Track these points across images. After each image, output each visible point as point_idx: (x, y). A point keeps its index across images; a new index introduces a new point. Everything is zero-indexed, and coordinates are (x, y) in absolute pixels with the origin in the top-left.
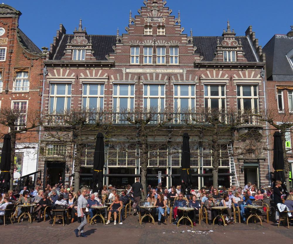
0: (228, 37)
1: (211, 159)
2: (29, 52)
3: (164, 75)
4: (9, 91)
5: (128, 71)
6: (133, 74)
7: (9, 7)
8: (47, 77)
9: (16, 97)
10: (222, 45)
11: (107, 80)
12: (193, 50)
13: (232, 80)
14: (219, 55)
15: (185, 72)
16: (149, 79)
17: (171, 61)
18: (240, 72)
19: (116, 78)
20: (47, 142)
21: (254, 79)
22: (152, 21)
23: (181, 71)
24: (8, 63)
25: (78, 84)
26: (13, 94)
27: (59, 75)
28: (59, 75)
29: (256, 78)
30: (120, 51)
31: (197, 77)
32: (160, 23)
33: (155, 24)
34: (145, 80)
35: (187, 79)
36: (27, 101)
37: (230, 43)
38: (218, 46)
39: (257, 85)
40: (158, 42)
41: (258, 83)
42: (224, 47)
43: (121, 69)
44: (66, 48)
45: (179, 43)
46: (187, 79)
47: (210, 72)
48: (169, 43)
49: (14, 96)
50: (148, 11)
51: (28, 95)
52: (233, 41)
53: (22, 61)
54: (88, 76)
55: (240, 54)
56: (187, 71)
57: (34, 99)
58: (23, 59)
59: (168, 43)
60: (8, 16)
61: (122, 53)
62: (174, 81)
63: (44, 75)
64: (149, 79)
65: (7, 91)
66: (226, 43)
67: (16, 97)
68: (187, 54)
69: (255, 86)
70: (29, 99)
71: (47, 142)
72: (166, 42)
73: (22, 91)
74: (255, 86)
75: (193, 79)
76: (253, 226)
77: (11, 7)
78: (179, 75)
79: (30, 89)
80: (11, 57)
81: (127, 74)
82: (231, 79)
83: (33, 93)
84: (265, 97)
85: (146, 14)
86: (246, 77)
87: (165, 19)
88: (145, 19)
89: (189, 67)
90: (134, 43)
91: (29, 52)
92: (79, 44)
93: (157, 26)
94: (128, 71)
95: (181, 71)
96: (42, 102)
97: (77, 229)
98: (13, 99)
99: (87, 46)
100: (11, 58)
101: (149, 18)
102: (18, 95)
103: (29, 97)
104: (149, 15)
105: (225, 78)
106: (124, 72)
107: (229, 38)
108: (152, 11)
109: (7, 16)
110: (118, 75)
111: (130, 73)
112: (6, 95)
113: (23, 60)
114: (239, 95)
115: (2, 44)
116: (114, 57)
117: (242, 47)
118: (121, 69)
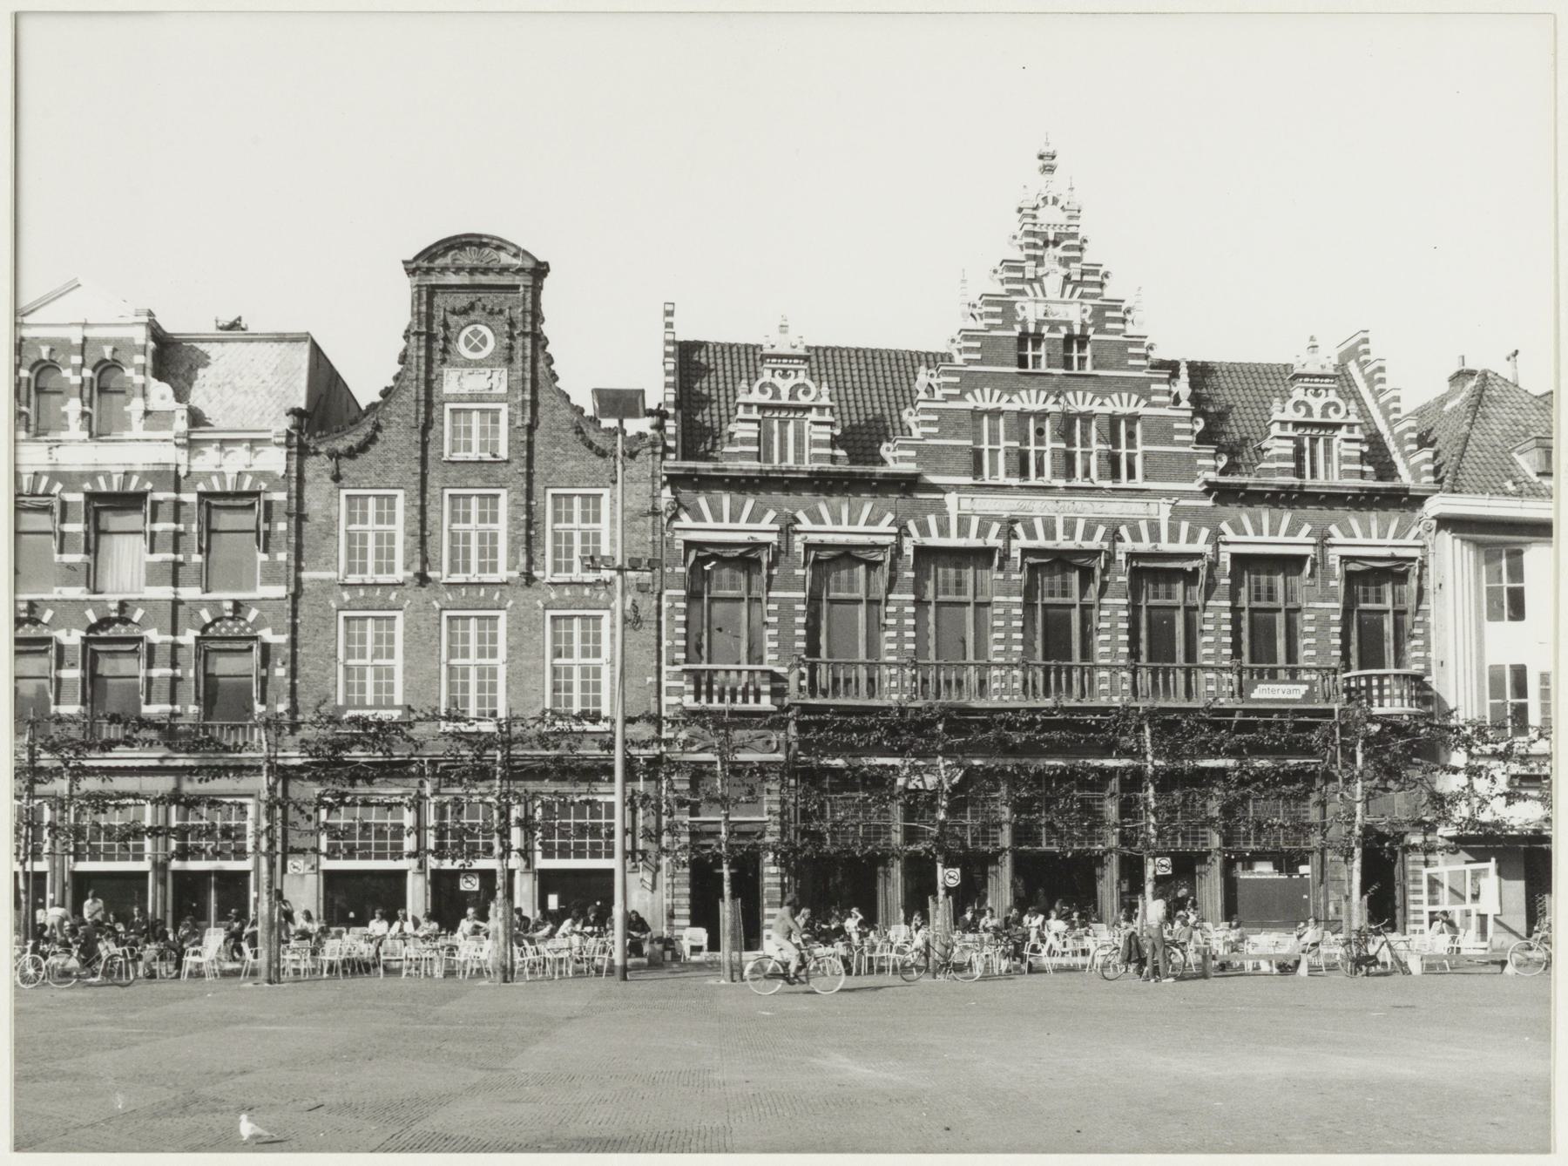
1: (1149, 758)
8: (676, 524)
12: (1192, 432)
17: (1169, 480)
27: (1367, 534)
28: (1367, 534)
29: (1295, 535)
35: (1174, 536)
40: (1066, 399)
44: (1366, 449)
46: (1174, 536)
47: (1272, 518)
52: (1327, 400)
54: (1353, 536)
59: (1056, 402)
75: (1192, 538)
76: (156, 986)
82: (1323, 542)
86: (840, 523)
97: (1307, 863)
99: (814, 410)
102: (362, 592)
103: (401, 597)
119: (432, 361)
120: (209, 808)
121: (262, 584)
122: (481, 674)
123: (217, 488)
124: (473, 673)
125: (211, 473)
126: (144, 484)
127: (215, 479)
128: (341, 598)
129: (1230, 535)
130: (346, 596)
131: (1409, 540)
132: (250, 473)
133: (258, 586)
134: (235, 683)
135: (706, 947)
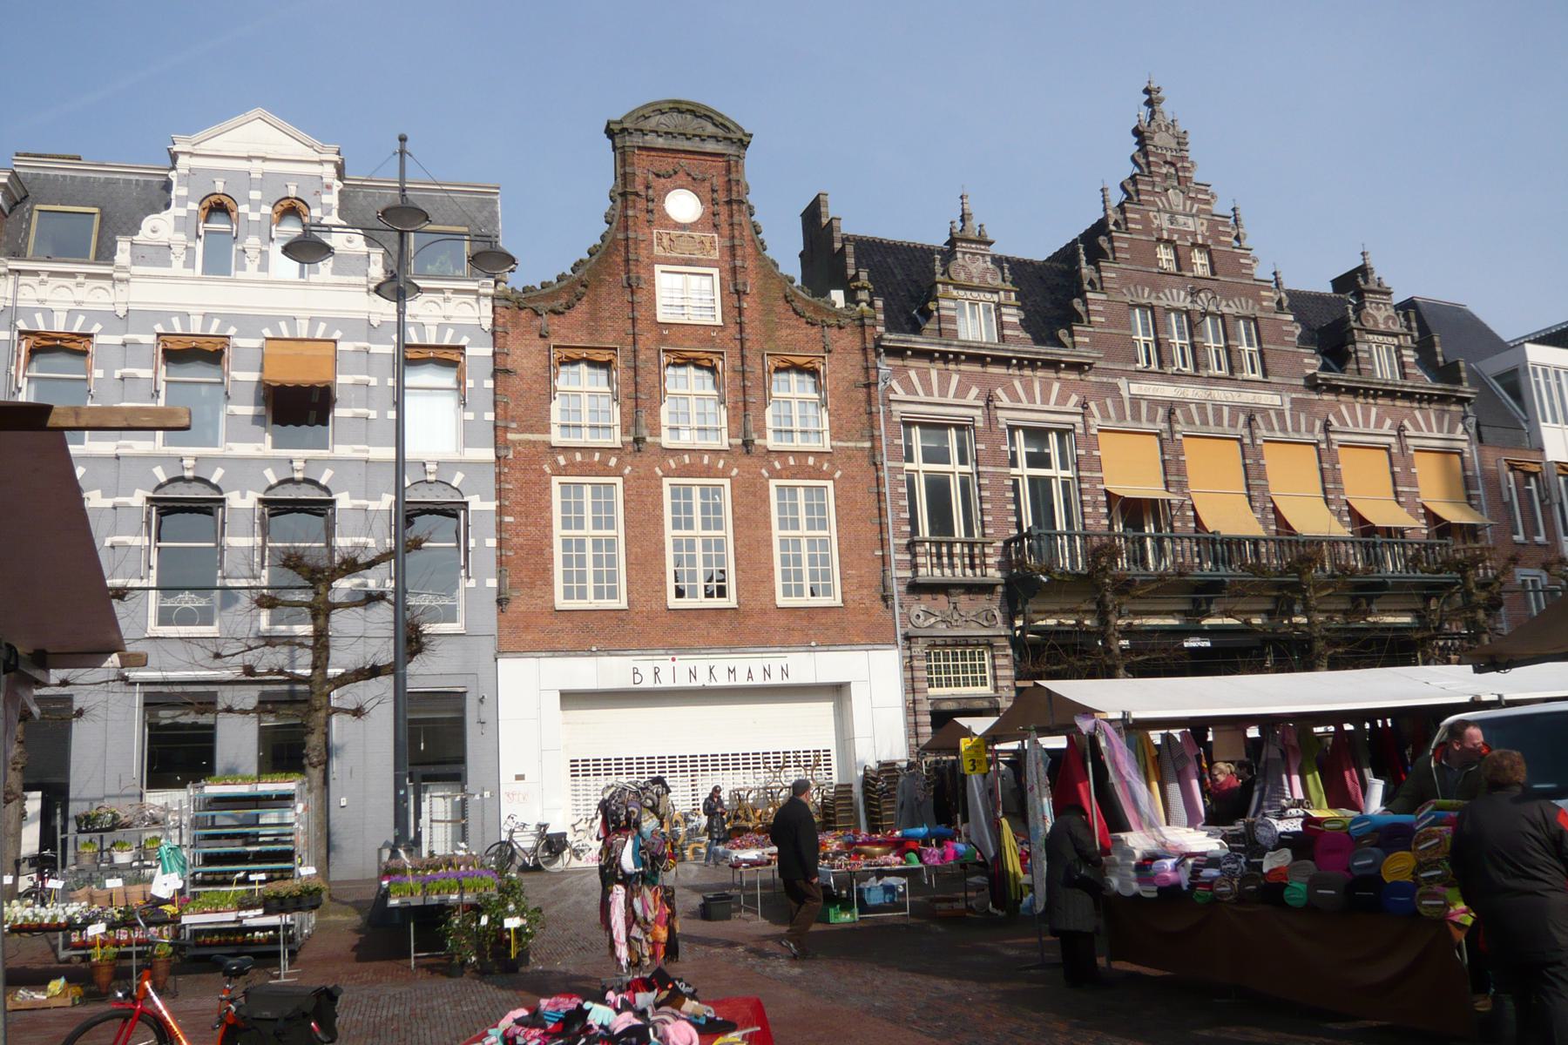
0: (971, 253)
2: (807, 297)
3: (1235, 409)
4: (756, 442)
5: (1135, 389)
6: (1154, 403)
7: (712, 115)
9: (786, 467)
10: (952, 279)
11: (1079, 418)
13: (1403, 438)
14: (943, 312)
15: (1287, 406)
16: (1197, 422)
18: (1417, 413)
19: (1105, 415)
20: (929, 641)
21: (1057, 408)
22: (1172, 223)
23: (1276, 400)
24: (733, 330)
25: (993, 429)
26: (774, 455)
30: (1103, 320)
31: (1318, 424)
32: (1194, 234)
33: (1183, 235)
34: (1187, 423)
36: (727, 482)
37: (1381, 320)
38: (940, 283)
39: (1068, 431)
41: (1074, 425)
42: (958, 287)
43: (1115, 381)
45: (1257, 307)
48: (1231, 303)
49: (777, 465)
50: (1157, 190)
51: (829, 461)
53: (789, 331)
54: (1020, 401)
55: (1012, 316)
56: (1293, 401)
57: (853, 478)
58: (790, 322)
60: (710, 146)
61: (1109, 327)
62: (1264, 432)
63: (879, 389)
64: (1197, 422)
65: (747, 444)
66: (1372, 322)
67: (786, 467)
68: (1282, 344)
69: (1061, 433)
70: (838, 475)
71: (929, 641)
72: (1154, 295)
73: (800, 444)
74: (1061, 433)
77: (721, 116)
78: (1272, 413)
79: (832, 438)
80: (740, 311)
81: (1136, 401)
83: (849, 455)
84: (1480, 492)
85: (1152, 199)
87: (1205, 222)
88: (1151, 214)
89: (1294, 388)
90: (1138, 296)
91: (807, 297)
92: (976, 282)
93: (1189, 244)
94: (1135, 389)
95: (1276, 400)
96: (887, 490)
98: (560, 471)
100: (740, 315)
101: (1162, 214)
102: (687, 459)
103: (834, 467)
104: (1161, 206)
105: (1070, 407)
106: (1125, 394)
107: (1378, 303)
108: (1167, 190)
109: (708, 150)
110: (1109, 401)
111: (1142, 397)
112: (746, 460)
113: (789, 326)
114: (909, 458)
115: (701, 256)
116: (1087, 340)
117: (1015, 292)
118: (1115, 381)
119: (691, 259)
120: (1126, 828)
121: (90, 440)
122: (706, 546)
123: (42, 328)
124: (699, 544)
125: (37, 310)
126: (334, 332)
127: (39, 317)
128: (556, 462)
129: (1005, 401)
130: (562, 460)
131: (1070, 407)
132: (451, 325)
133: (86, 442)
134: (1196, 581)
135: (664, 967)
